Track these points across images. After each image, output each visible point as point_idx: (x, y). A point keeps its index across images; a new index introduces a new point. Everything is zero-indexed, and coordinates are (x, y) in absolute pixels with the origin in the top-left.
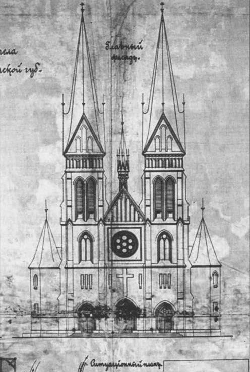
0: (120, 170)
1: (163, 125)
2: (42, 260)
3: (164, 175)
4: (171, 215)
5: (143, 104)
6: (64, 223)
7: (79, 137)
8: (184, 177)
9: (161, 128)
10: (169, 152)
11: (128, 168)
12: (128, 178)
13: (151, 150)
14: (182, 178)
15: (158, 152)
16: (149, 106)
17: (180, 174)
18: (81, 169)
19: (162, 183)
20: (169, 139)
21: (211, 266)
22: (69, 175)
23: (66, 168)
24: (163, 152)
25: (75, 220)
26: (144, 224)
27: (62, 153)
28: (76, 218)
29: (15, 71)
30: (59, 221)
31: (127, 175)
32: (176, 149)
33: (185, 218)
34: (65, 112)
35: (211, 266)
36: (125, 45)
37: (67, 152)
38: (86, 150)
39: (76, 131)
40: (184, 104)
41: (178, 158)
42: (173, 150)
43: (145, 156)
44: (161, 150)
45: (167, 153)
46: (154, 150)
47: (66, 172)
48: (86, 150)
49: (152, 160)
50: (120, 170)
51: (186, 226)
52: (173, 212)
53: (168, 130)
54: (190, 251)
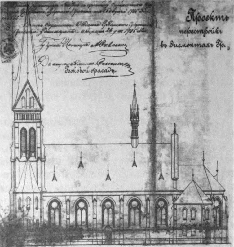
0: (132, 120)
1: (28, 89)
2: (187, 188)
3: (28, 126)
4: (33, 154)
5: (13, 73)
6: (13, 160)
7: (23, 97)
8: (42, 127)
9: (26, 91)
10: (32, 109)
11: (138, 118)
12: (138, 126)
13: (19, 106)
14: (39, 127)
15: (24, 109)
16: (38, 74)
17: (38, 125)
18: (25, 121)
19: (26, 132)
20: (32, 99)
21: (34, 193)
22: (17, 125)
23: (15, 119)
24: (28, 109)
25: (20, 158)
26: (37, 161)
27: (11, 108)
28: (21, 156)
29: (211, 33)
30: (9, 159)
31: (138, 124)
32: (37, 107)
33: (43, 157)
34: (14, 79)
35: (34, 193)
36: (148, 14)
37: (15, 108)
38: (29, 107)
39: (22, 92)
40: (42, 72)
41: (21, 113)
42: (35, 107)
43: (14, 111)
44: (26, 107)
45: (30, 109)
46: (21, 107)
47: (15, 123)
48: (29, 107)
49: (38, 115)
50: (132, 120)
51: (43, 163)
52: (35, 152)
53: (31, 93)
54: (196, 185)
